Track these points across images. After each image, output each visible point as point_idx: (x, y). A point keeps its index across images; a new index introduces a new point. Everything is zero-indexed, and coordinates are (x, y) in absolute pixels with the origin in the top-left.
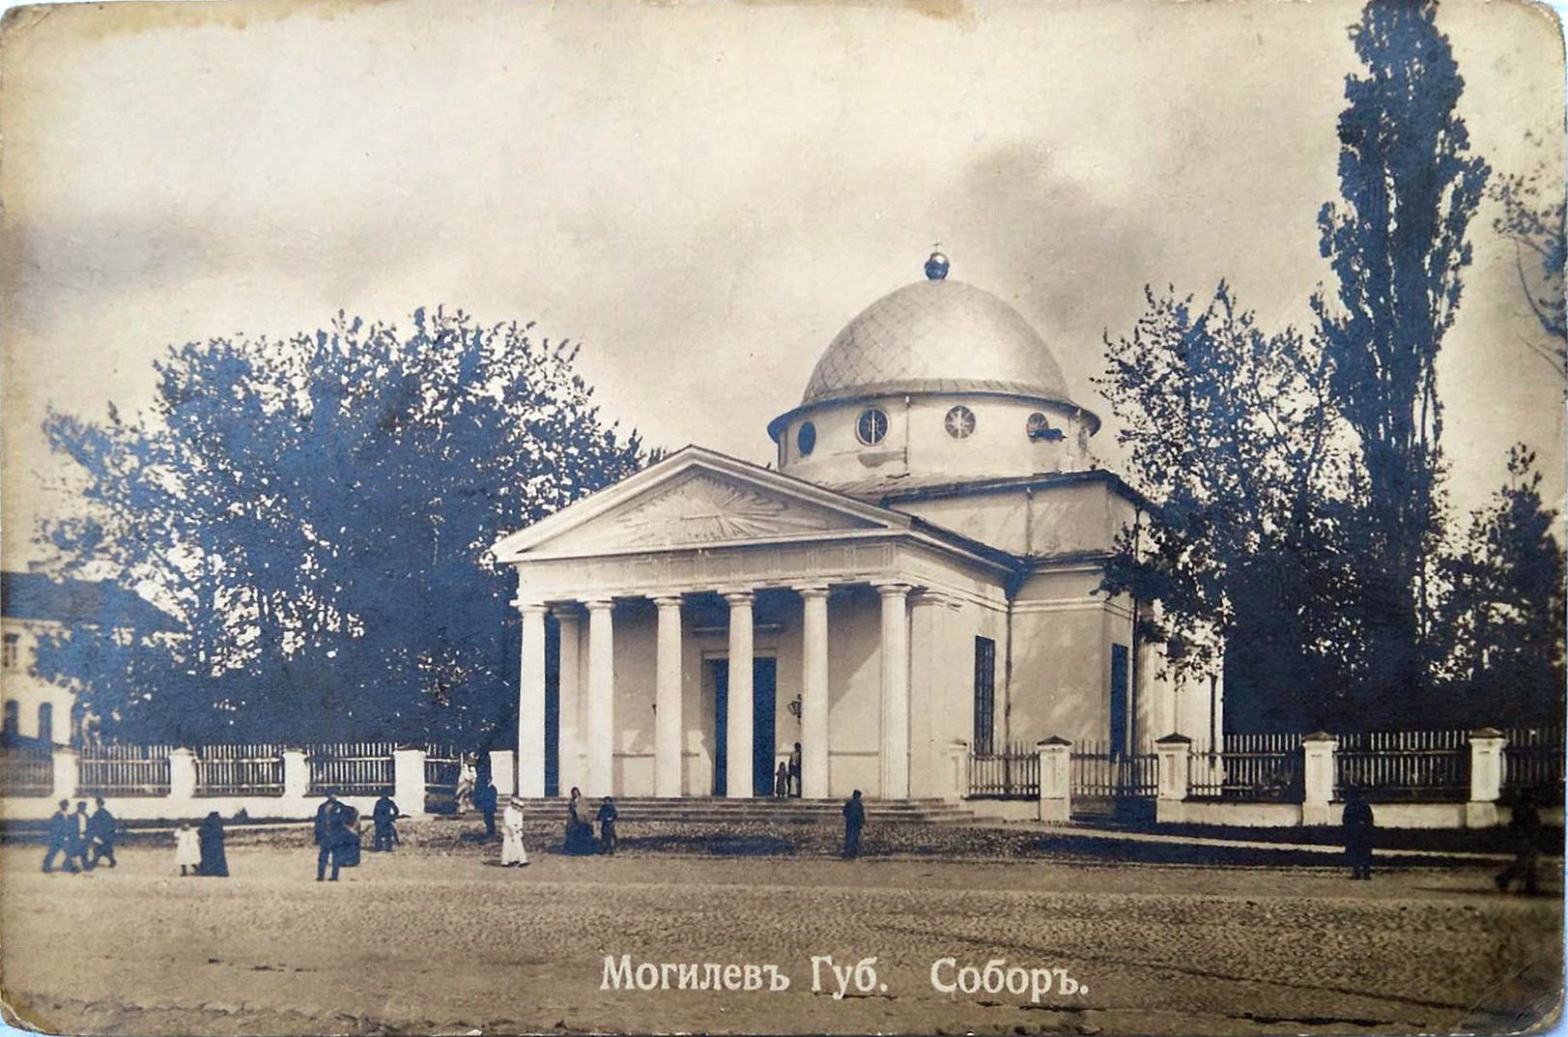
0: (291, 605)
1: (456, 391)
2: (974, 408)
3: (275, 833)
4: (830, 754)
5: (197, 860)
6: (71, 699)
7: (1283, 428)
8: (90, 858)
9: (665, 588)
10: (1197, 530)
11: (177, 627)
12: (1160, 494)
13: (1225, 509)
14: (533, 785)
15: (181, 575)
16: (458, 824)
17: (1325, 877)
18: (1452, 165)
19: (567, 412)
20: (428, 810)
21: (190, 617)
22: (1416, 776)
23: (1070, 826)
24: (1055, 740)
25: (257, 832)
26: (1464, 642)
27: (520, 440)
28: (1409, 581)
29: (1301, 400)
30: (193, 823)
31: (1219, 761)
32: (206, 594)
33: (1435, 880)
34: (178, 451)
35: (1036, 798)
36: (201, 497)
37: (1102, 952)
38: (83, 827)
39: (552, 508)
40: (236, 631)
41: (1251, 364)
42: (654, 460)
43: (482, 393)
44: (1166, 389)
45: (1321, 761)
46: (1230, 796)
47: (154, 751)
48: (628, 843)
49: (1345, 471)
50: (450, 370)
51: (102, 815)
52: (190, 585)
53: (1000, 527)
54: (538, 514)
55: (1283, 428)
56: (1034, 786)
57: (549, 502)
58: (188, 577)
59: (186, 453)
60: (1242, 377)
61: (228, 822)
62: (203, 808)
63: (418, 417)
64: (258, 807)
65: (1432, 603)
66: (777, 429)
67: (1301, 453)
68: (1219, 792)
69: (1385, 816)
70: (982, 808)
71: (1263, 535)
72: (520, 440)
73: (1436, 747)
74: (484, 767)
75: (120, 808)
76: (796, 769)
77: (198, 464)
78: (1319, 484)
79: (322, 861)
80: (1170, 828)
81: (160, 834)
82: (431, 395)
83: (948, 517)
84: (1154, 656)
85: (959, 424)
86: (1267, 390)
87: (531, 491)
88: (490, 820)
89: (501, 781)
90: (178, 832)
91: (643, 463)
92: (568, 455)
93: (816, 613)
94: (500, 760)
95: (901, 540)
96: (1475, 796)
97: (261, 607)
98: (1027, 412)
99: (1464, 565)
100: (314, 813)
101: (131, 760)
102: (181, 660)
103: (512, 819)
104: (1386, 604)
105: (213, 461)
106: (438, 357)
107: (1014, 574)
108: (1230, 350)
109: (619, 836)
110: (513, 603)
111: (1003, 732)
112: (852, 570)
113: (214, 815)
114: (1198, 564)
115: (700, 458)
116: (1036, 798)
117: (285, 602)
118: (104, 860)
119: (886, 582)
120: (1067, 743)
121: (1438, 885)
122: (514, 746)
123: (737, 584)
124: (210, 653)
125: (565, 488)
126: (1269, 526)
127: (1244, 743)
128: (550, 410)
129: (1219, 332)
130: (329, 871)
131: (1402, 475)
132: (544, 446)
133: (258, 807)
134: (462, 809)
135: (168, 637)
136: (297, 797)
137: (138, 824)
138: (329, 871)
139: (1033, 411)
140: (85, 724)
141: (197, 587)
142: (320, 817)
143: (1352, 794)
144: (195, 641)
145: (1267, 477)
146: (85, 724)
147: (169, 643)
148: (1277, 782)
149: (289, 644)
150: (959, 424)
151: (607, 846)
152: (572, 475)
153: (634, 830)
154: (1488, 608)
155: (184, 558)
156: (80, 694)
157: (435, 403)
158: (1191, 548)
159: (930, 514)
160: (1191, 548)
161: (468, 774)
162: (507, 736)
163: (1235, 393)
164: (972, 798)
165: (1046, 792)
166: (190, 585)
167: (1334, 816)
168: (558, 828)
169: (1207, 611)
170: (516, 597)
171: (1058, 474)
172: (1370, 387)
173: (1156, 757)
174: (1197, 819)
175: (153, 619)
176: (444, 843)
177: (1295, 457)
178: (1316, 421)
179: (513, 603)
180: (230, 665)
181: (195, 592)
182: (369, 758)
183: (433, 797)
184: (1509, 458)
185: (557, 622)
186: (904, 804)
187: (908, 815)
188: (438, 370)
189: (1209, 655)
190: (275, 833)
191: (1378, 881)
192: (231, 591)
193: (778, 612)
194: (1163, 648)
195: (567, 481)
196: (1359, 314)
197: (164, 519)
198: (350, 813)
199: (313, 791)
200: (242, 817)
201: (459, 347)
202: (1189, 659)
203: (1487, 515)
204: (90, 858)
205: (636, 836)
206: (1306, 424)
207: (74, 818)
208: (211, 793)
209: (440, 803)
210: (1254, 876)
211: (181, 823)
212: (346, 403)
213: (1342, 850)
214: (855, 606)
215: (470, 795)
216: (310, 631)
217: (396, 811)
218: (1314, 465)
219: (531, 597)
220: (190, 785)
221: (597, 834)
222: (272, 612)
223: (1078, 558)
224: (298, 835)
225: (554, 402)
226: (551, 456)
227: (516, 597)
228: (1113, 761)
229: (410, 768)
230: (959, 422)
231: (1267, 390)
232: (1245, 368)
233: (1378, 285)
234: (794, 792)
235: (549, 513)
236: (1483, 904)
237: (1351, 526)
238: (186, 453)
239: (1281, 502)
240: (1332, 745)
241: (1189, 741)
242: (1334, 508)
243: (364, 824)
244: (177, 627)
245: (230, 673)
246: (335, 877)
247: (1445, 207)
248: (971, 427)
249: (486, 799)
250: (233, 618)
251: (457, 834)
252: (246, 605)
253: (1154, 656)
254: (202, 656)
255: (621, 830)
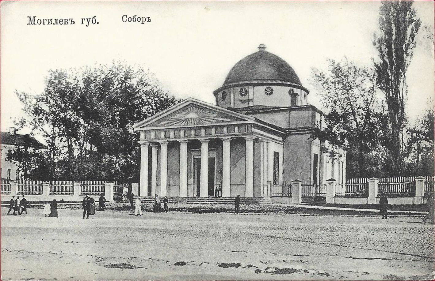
0: (77, 142)
1: (123, 82)
2: (272, 87)
3: (71, 205)
4: (231, 184)
5: (50, 213)
6: (17, 168)
7: (362, 93)
8: (20, 212)
10: (337, 121)
11: (47, 148)
12: (327, 111)
13: (345, 116)
14: (144, 192)
15: (47, 133)
16: (122, 204)
17: (374, 218)
18: (411, 21)
19: (155, 88)
20: (114, 199)
21: (49, 144)
22: (400, 190)
25: (66, 205)
26: (414, 152)
27: (141, 96)
28: (398, 135)
29: (368, 84)
30: (49, 202)
31: (344, 186)
32: (53, 139)
33: (405, 219)
34: (47, 98)
36: (53, 111)
37: (309, 240)
38: (19, 203)
39: (150, 115)
40: (62, 149)
41: (354, 75)
42: (179, 102)
43: (130, 83)
44: (329, 82)
45: (374, 186)
46: (347, 196)
47: (38, 182)
48: (172, 210)
49: (381, 105)
50: (122, 76)
51: (24, 200)
52: (49, 136)
54: (146, 117)
55: (362, 93)
56: (290, 193)
57: (149, 113)
58: (48, 134)
59: (49, 98)
60: (351, 79)
61: (58, 202)
62: (51, 198)
63: (113, 89)
64: (67, 198)
65: (405, 141)
66: (216, 93)
67: (368, 100)
68: (344, 195)
69: (391, 201)
71: (357, 123)
72: (141, 96)
73: (406, 182)
74: (130, 188)
75: (29, 198)
76: (221, 189)
77: (52, 102)
78: (373, 108)
79: (84, 213)
81: (40, 205)
82: (116, 83)
83: (267, 118)
84: (326, 157)
86: (358, 81)
87: (144, 110)
88: (132, 202)
89: (135, 192)
90: (44, 205)
91: (176, 102)
92: (155, 100)
94: (135, 186)
96: (416, 196)
97: (68, 142)
99: (412, 132)
100: (82, 200)
101: (32, 183)
102: (46, 157)
103: (137, 203)
104: (391, 143)
105: (56, 101)
106: (119, 72)
108: (347, 71)
109: (169, 207)
113: (55, 200)
114: (338, 131)
115: (193, 101)
117: (75, 141)
118: (24, 212)
121: (407, 221)
124: (54, 155)
125: (154, 109)
126: (358, 120)
127: (352, 181)
129: (344, 66)
130: (86, 216)
131: (396, 105)
132: (148, 97)
133: (67, 198)
134: (124, 199)
135: (43, 150)
136: (77, 196)
137: (34, 202)
138: (86, 216)
140: (20, 175)
141: (51, 136)
142: (84, 202)
143: (383, 196)
144: (50, 152)
145: (358, 106)
146: (20, 175)
147: (43, 152)
148: (361, 192)
149: (76, 153)
151: (166, 210)
152: (156, 106)
153: (173, 206)
154: (420, 143)
155: (48, 127)
156: (20, 167)
157: (118, 85)
158: (336, 126)
160: (336, 126)
161: (125, 190)
162: (137, 180)
163: (349, 83)
166: (49, 136)
167: (376, 201)
168: (151, 205)
169: (340, 144)
172: (388, 80)
175: (37, 145)
176: (118, 209)
177: (366, 101)
178: (372, 90)
180: (60, 159)
181: (51, 138)
182: (97, 185)
183: (116, 196)
184: (427, 101)
185: (151, 148)
188: (118, 76)
189: (341, 156)
190: (71, 205)
191: (389, 219)
192: (61, 138)
193: (216, 145)
194: (329, 154)
195: (155, 108)
196: (385, 62)
197: (42, 117)
198: (92, 200)
199: (83, 193)
200: (62, 201)
201: (124, 70)
202: (335, 157)
203: (420, 116)
204: (20, 212)
205: (174, 207)
206: (369, 92)
207: (16, 200)
208: (53, 194)
209: (118, 199)
210: (355, 218)
211: (45, 202)
212: (93, 85)
213: (379, 211)
214: (238, 143)
215: (126, 196)
216: (82, 150)
217: (105, 200)
218: (371, 103)
220: (49, 192)
221: (163, 207)
222: (71, 143)
224: (77, 206)
225: (151, 85)
226: (150, 100)
228: (313, 186)
229: (110, 189)
231: (358, 81)
232: (351, 76)
233: (390, 54)
234: (220, 195)
235: (149, 116)
236: (419, 226)
237: (381, 119)
238: (49, 98)
239: (362, 113)
240: (377, 181)
241: (336, 180)
242: (376, 115)
243: (96, 203)
244: (47, 148)
245: (59, 161)
246: (87, 218)
247: (409, 32)
248: (272, 93)
249: (130, 197)
250: (61, 146)
251: (122, 207)
252: (64, 142)
253: (326, 157)
254: (52, 156)
255: (169, 206)
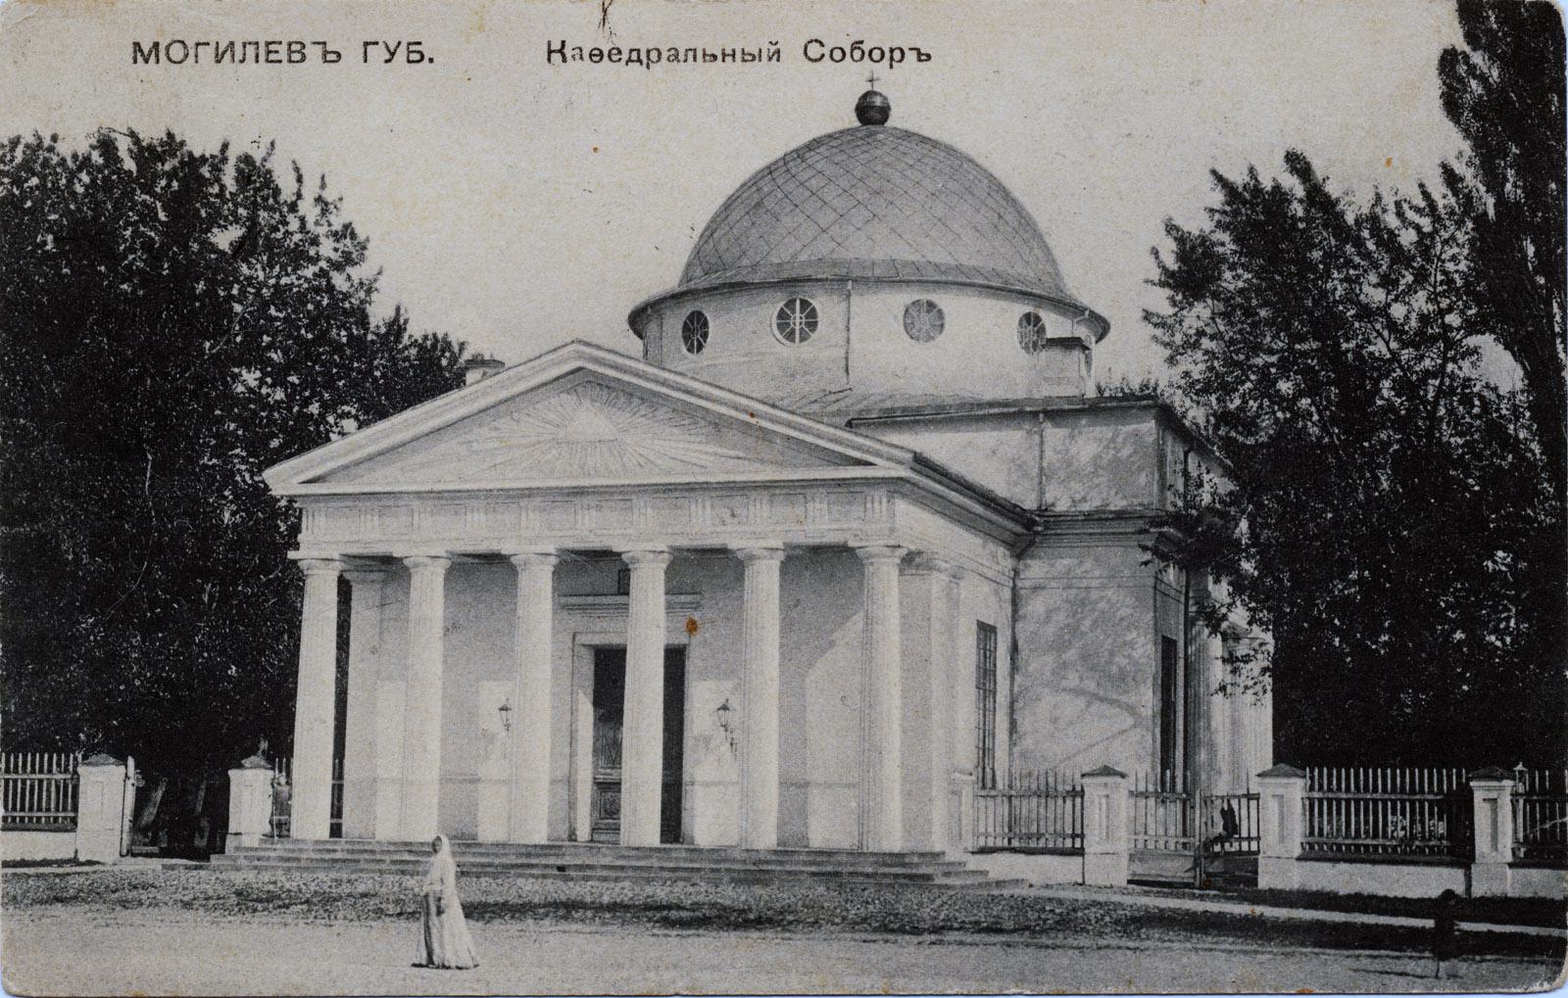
2: (944, 300)
9: (535, 541)
23: (1123, 892)
24: (1107, 771)
35: (1080, 852)
53: (984, 457)
56: (1074, 836)
70: (1001, 866)
80: (1276, 898)
85: (925, 321)
93: (765, 581)
95: (895, 486)
98: (1023, 308)
107: (1026, 530)
110: (292, 555)
111: (1276, 819)
112: (821, 522)
116: (1080, 852)
119: (874, 545)
120: (1123, 776)
122: (280, 753)
123: (645, 538)
128: (309, 271)
139: (1028, 309)
150: (925, 321)
159: (937, 444)
164: (984, 851)
165: (1093, 843)
170: (296, 546)
171: (1082, 399)
173: (1256, 797)
174: (1314, 885)
179: (292, 555)
186: (898, 858)
187: (906, 872)
219: (321, 546)
223: (1120, 516)
227: (296, 546)
230: (797, 319)
248: (813, 325)
